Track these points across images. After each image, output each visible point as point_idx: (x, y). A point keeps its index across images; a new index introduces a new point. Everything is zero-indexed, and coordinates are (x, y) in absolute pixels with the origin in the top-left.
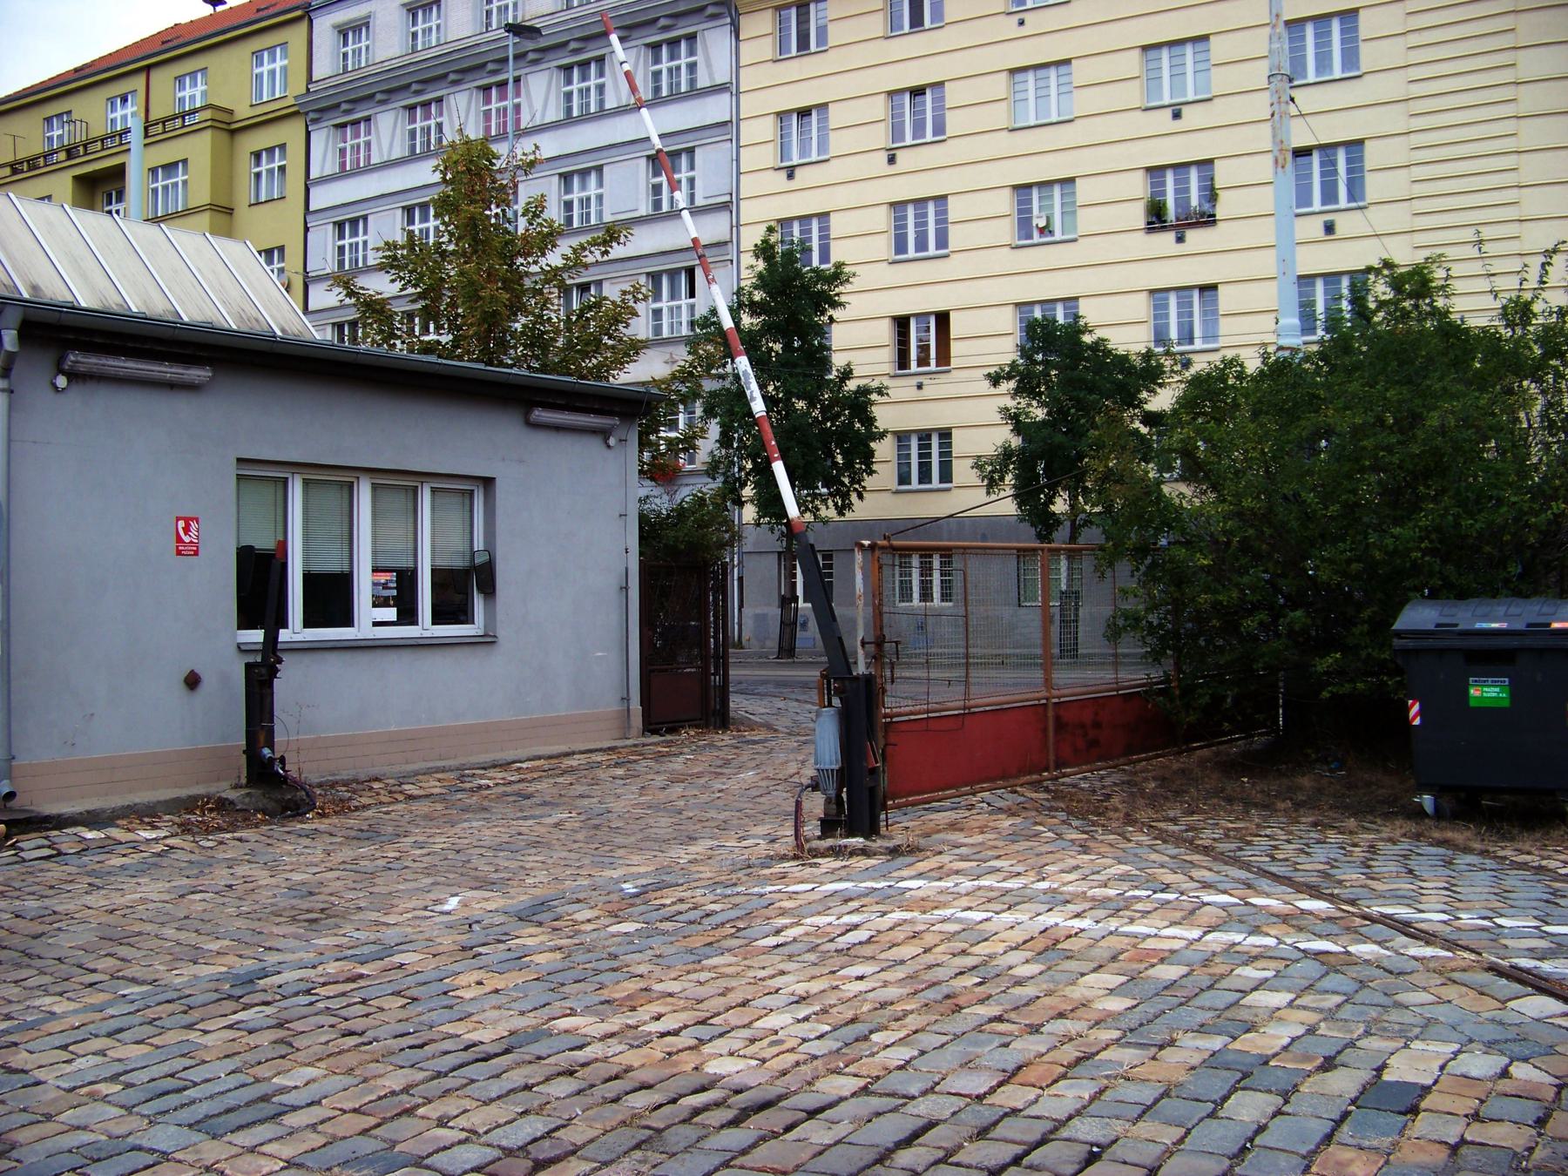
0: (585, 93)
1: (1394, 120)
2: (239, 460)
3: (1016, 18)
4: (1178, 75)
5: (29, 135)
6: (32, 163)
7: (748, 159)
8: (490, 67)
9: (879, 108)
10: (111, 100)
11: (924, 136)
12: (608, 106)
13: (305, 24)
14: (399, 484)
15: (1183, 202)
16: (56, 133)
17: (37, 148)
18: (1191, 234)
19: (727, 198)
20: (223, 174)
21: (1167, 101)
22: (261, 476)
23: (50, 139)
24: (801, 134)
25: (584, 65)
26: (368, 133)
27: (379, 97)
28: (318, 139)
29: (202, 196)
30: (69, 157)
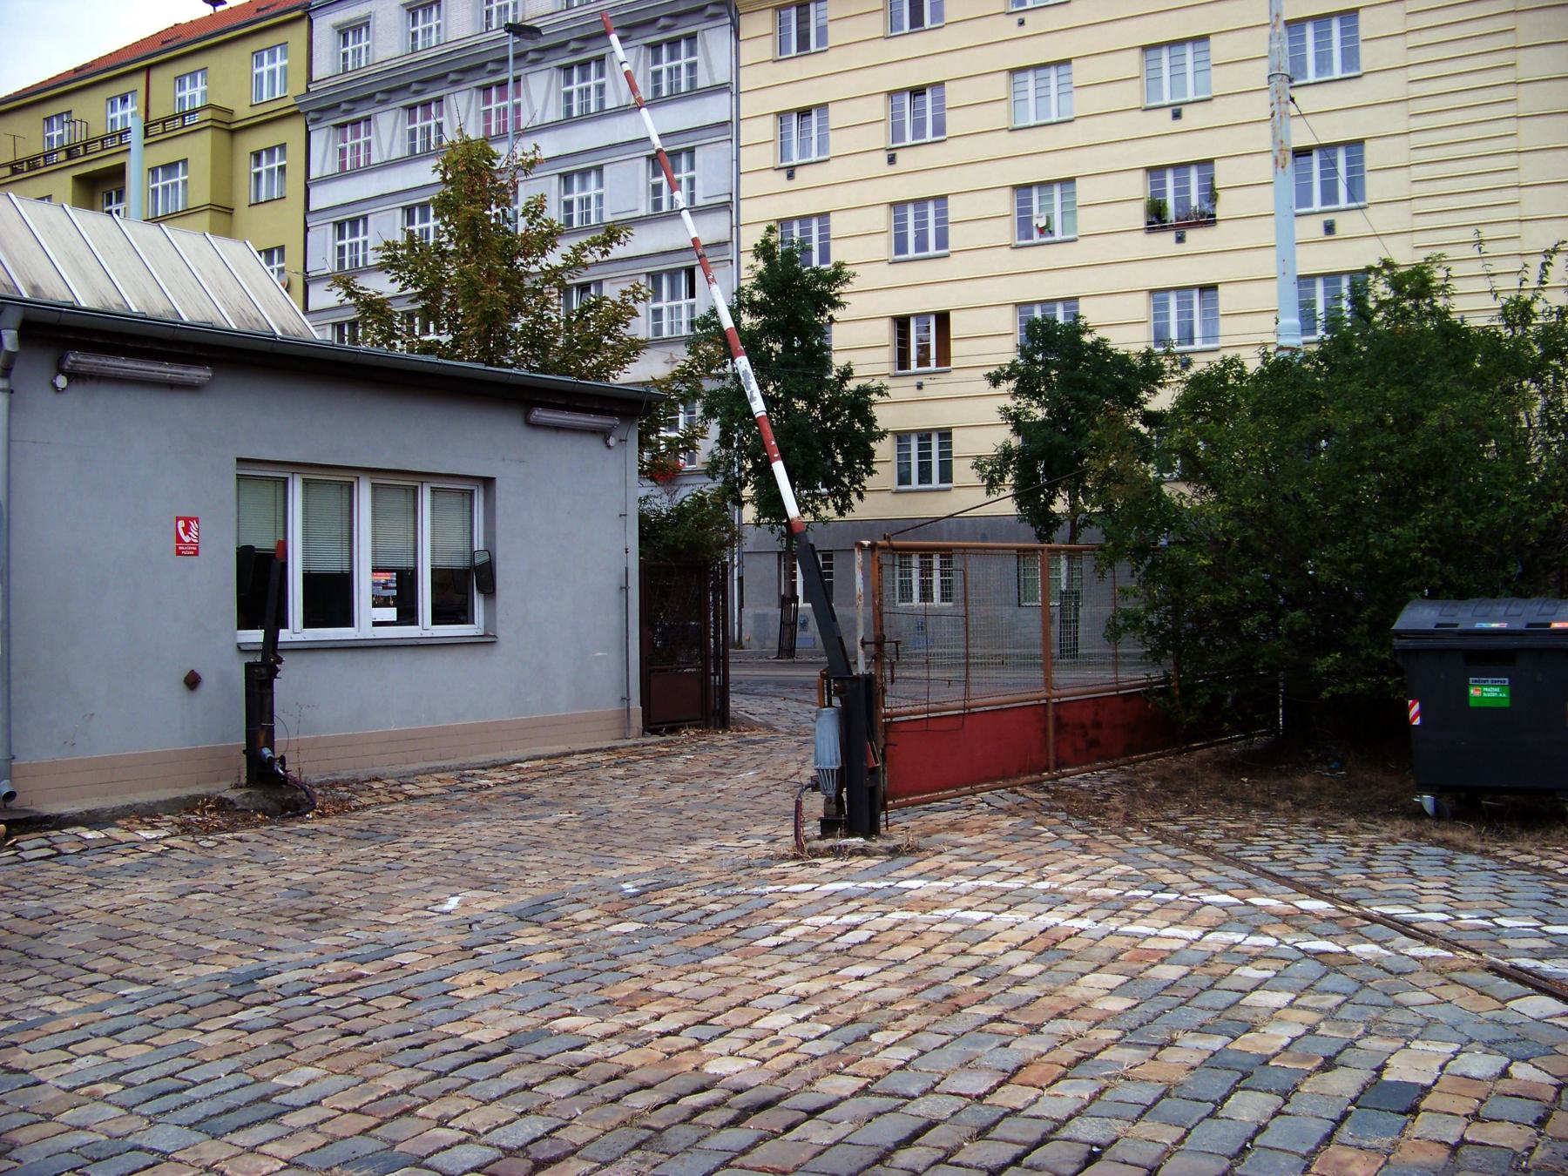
0: (585, 93)
1: (1394, 120)
2: (239, 460)
3: (1016, 18)
4: (1178, 75)
5: (29, 135)
6: (32, 163)
7: (748, 159)
8: (490, 67)
9: (879, 108)
10: (111, 100)
11: (924, 136)
12: (608, 106)
13: (305, 24)
14: (399, 484)
15: (1183, 202)
16: (56, 133)
17: (37, 148)
18: (1191, 234)
19: (727, 198)
20: (223, 174)
21: (1167, 101)
22: (261, 476)
23: (50, 139)
24: (801, 134)
25: (584, 65)
26: (368, 133)
27: (379, 97)
28: (318, 139)
29: (202, 196)
30: (69, 157)
